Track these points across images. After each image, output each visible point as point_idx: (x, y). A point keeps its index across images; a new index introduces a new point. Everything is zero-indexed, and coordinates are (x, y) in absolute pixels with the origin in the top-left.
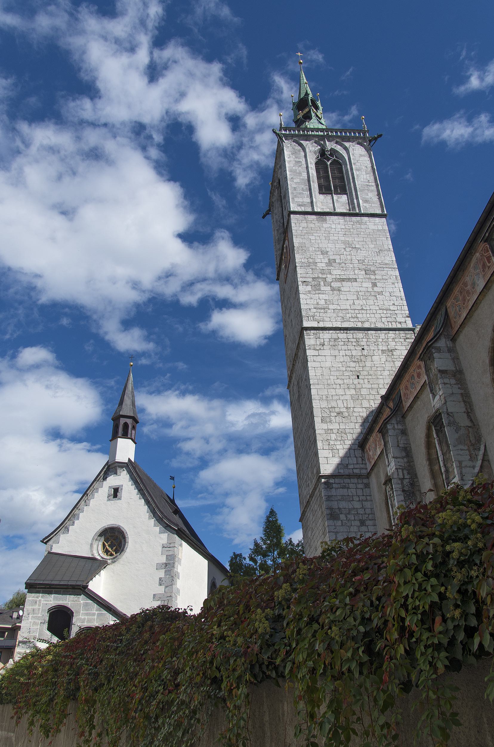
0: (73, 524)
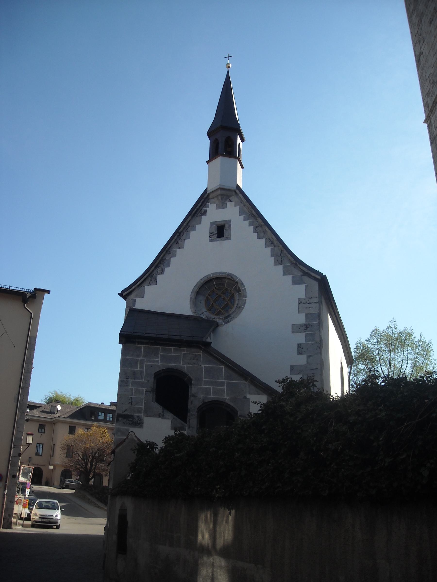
0: (162, 272)
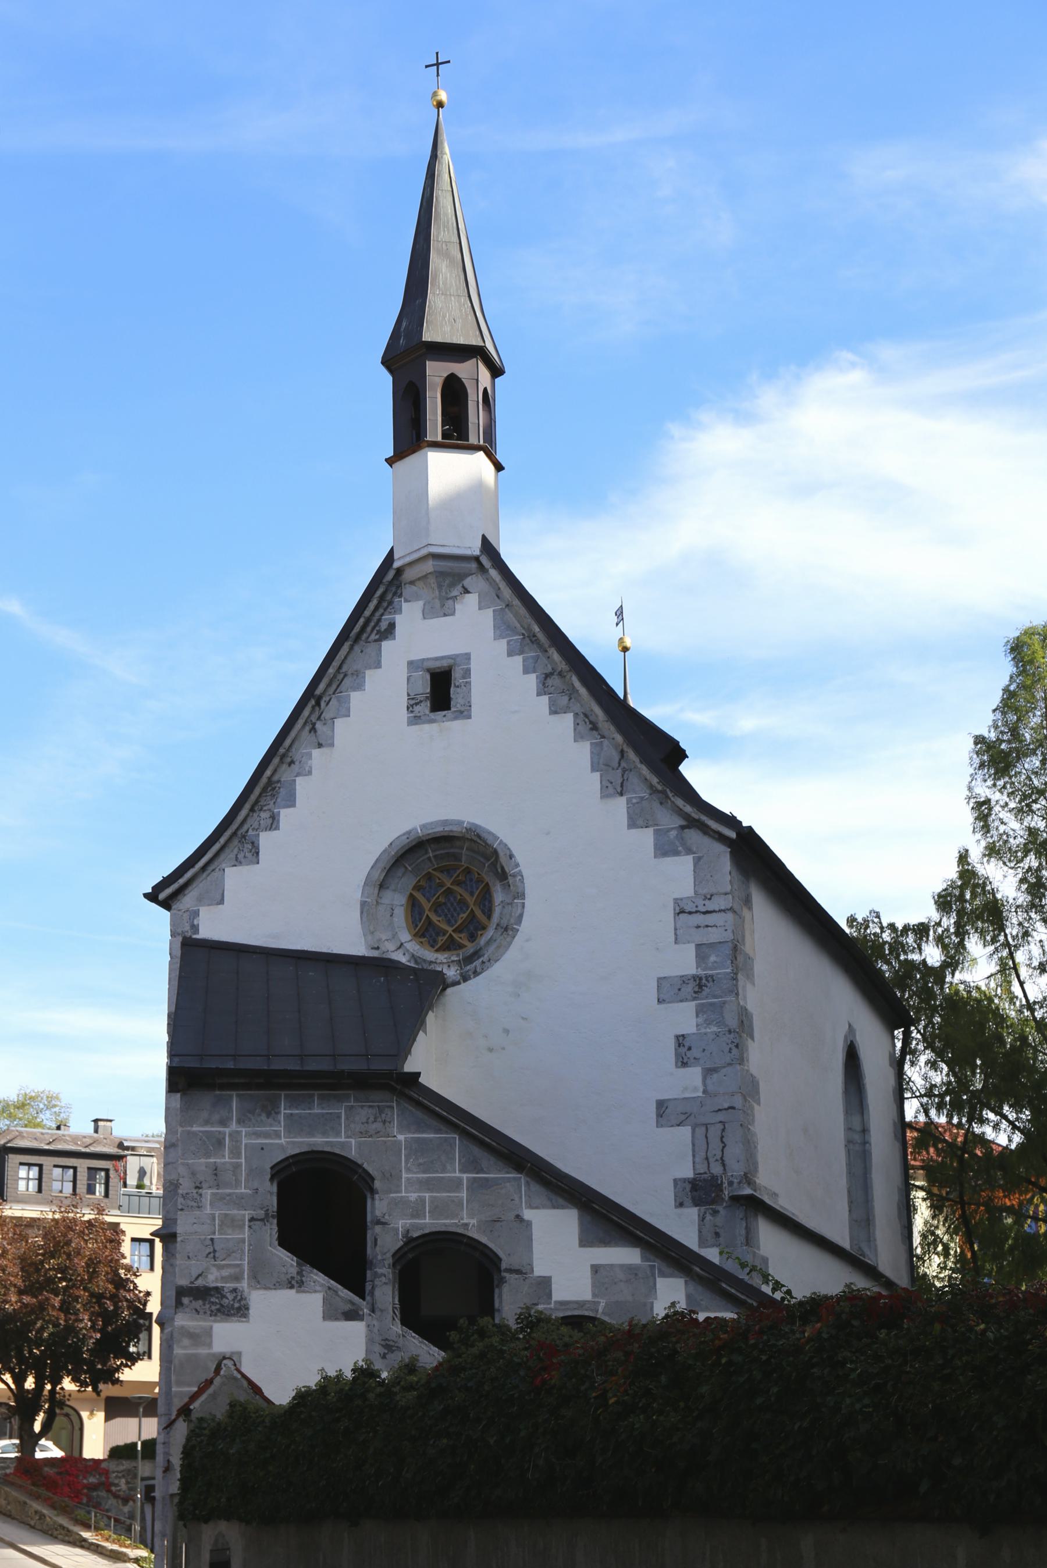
0: (274, 823)
